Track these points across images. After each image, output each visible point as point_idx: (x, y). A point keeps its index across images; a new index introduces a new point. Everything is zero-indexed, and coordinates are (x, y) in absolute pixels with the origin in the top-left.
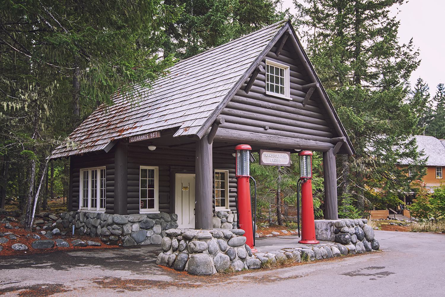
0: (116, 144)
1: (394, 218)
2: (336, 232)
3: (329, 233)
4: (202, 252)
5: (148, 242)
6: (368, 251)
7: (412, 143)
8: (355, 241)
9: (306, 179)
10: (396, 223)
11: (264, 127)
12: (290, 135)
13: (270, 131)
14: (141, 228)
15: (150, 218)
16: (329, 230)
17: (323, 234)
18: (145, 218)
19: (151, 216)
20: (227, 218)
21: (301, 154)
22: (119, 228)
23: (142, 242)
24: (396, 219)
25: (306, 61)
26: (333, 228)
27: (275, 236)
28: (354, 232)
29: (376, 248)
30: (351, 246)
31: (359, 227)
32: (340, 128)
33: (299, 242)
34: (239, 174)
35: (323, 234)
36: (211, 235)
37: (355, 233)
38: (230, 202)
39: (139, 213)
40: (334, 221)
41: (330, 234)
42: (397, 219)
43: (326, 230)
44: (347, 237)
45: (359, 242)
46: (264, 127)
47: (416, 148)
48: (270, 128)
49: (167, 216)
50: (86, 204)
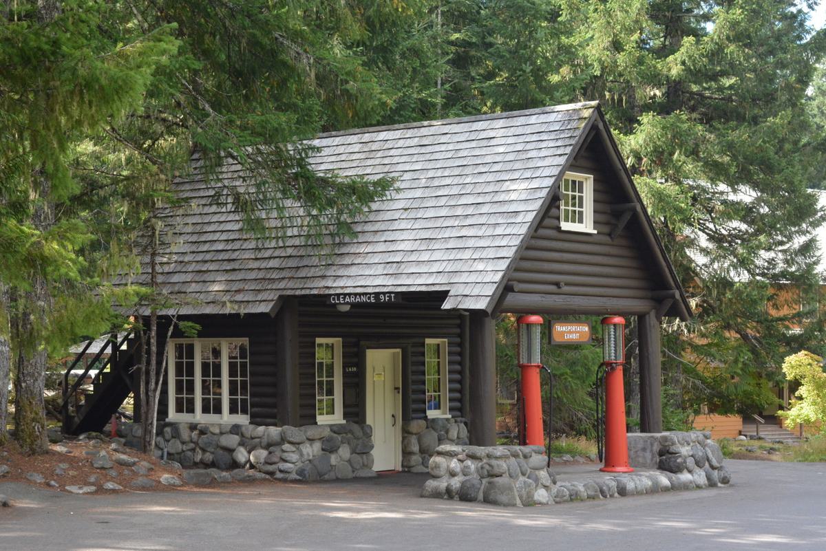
0: (286, 303)
1: (755, 434)
2: (661, 454)
3: (648, 455)
4: (501, 476)
5: (332, 475)
6: (712, 484)
7: (807, 248)
8: (691, 468)
9: (614, 365)
10: (761, 447)
11: (557, 284)
12: (598, 294)
13: (565, 289)
14: (323, 450)
15: (335, 432)
16: (648, 451)
17: (638, 456)
18: (327, 432)
19: (335, 428)
20: (447, 432)
21: (604, 321)
22: (294, 449)
23: (325, 474)
24: (760, 438)
25: (621, 168)
26: (656, 448)
27: (566, 462)
28: (691, 453)
29: (725, 481)
30: (685, 477)
31: (698, 445)
32: (669, 275)
33: (601, 470)
34: (524, 361)
35: (638, 456)
36: (509, 453)
37: (692, 456)
38: (450, 400)
39: (316, 423)
40: (658, 435)
41: (650, 457)
42: (762, 436)
43: (644, 449)
44: (679, 460)
45: (697, 470)
46: (557, 284)
47: (816, 263)
48: (566, 284)
49: (356, 428)
50: (186, 406)
